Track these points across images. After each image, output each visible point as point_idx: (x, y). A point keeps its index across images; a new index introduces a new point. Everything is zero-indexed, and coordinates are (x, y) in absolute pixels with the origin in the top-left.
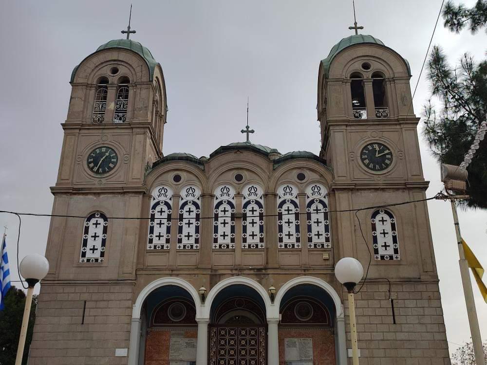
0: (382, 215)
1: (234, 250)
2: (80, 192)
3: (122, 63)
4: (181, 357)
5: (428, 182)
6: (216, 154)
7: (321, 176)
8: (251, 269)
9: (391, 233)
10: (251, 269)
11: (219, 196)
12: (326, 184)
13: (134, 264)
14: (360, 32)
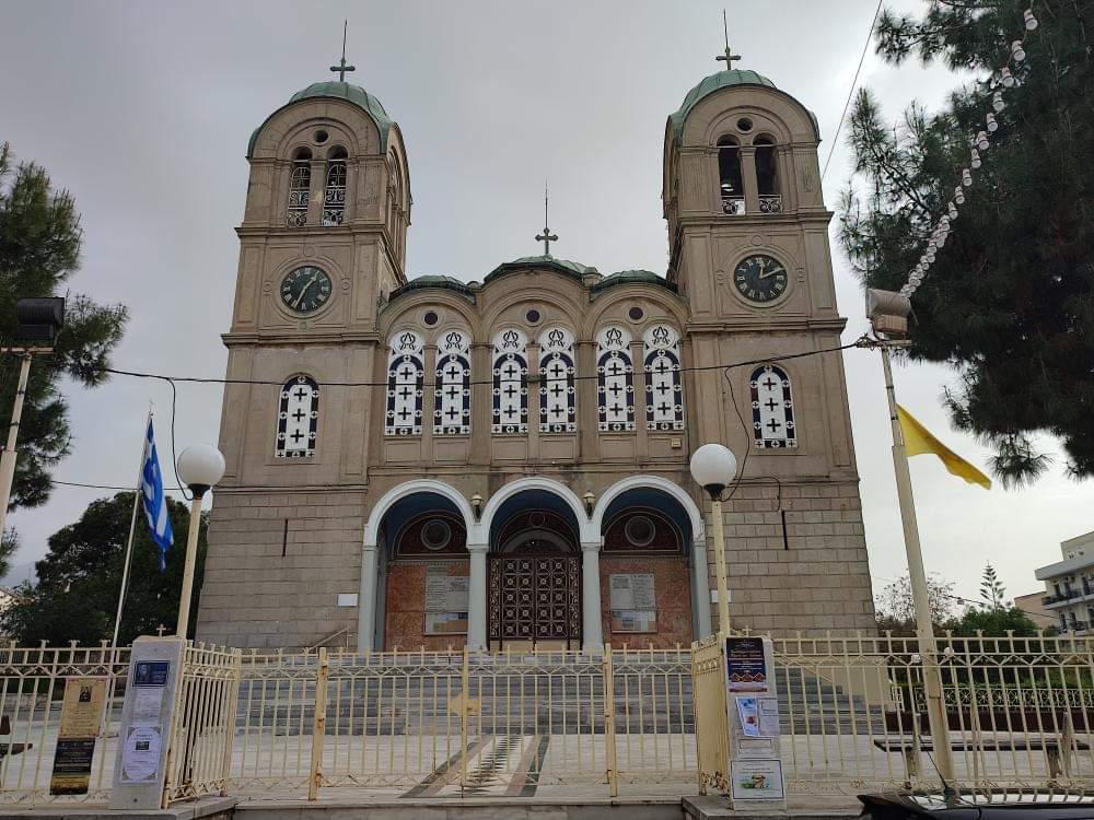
1: (526, 435)
2: (272, 342)
3: (335, 124)
4: (444, 606)
8: (555, 465)
9: (761, 405)
10: (555, 465)
12: (676, 325)
13: (365, 460)
14: (735, 65)
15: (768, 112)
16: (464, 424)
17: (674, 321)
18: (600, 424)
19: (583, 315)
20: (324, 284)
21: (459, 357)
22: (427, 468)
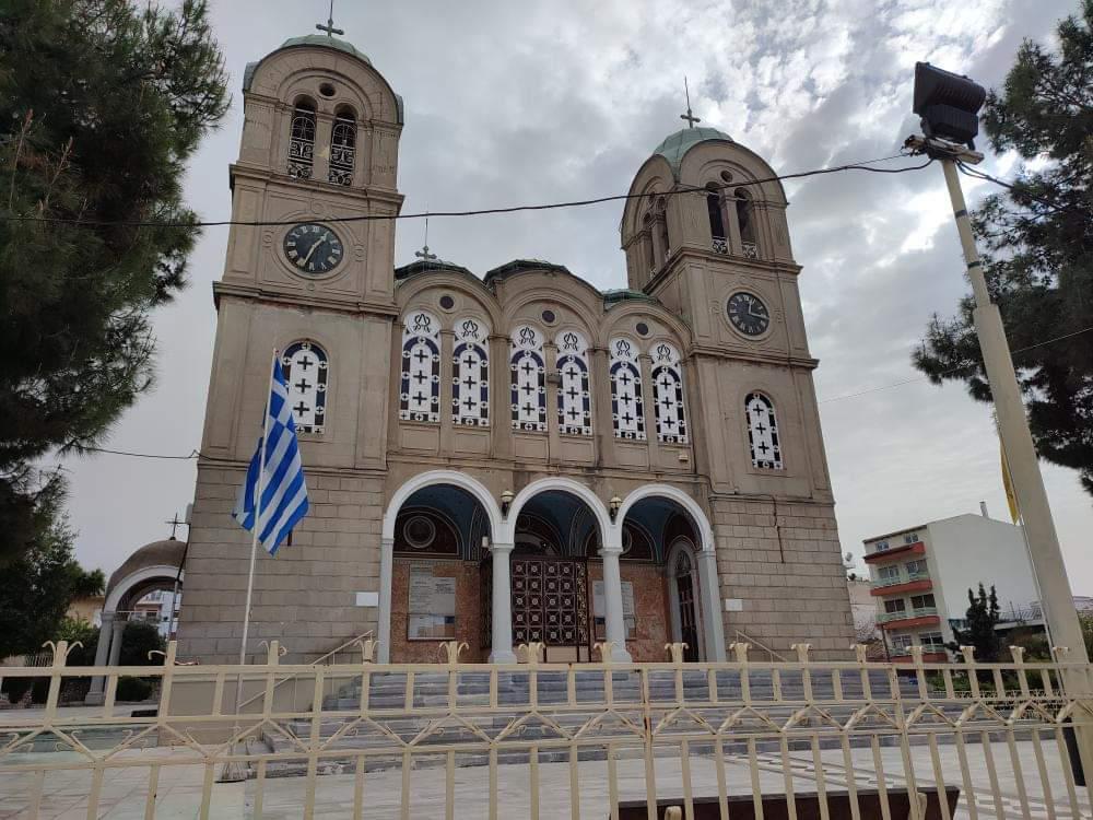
0: (305, 353)
1: (547, 435)
2: (275, 299)
3: (343, 80)
4: (429, 609)
5: (816, 362)
6: (502, 272)
7: (673, 331)
8: (577, 467)
9: (315, 386)
10: (577, 467)
11: (459, 335)
12: (679, 344)
13: (385, 443)
14: (695, 124)
15: (353, 82)
16: (482, 416)
17: (676, 341)
18: (402, 412)
19: (599, 323)
20: (335, 246)
21: (629, 364)
22: (450, 459)
